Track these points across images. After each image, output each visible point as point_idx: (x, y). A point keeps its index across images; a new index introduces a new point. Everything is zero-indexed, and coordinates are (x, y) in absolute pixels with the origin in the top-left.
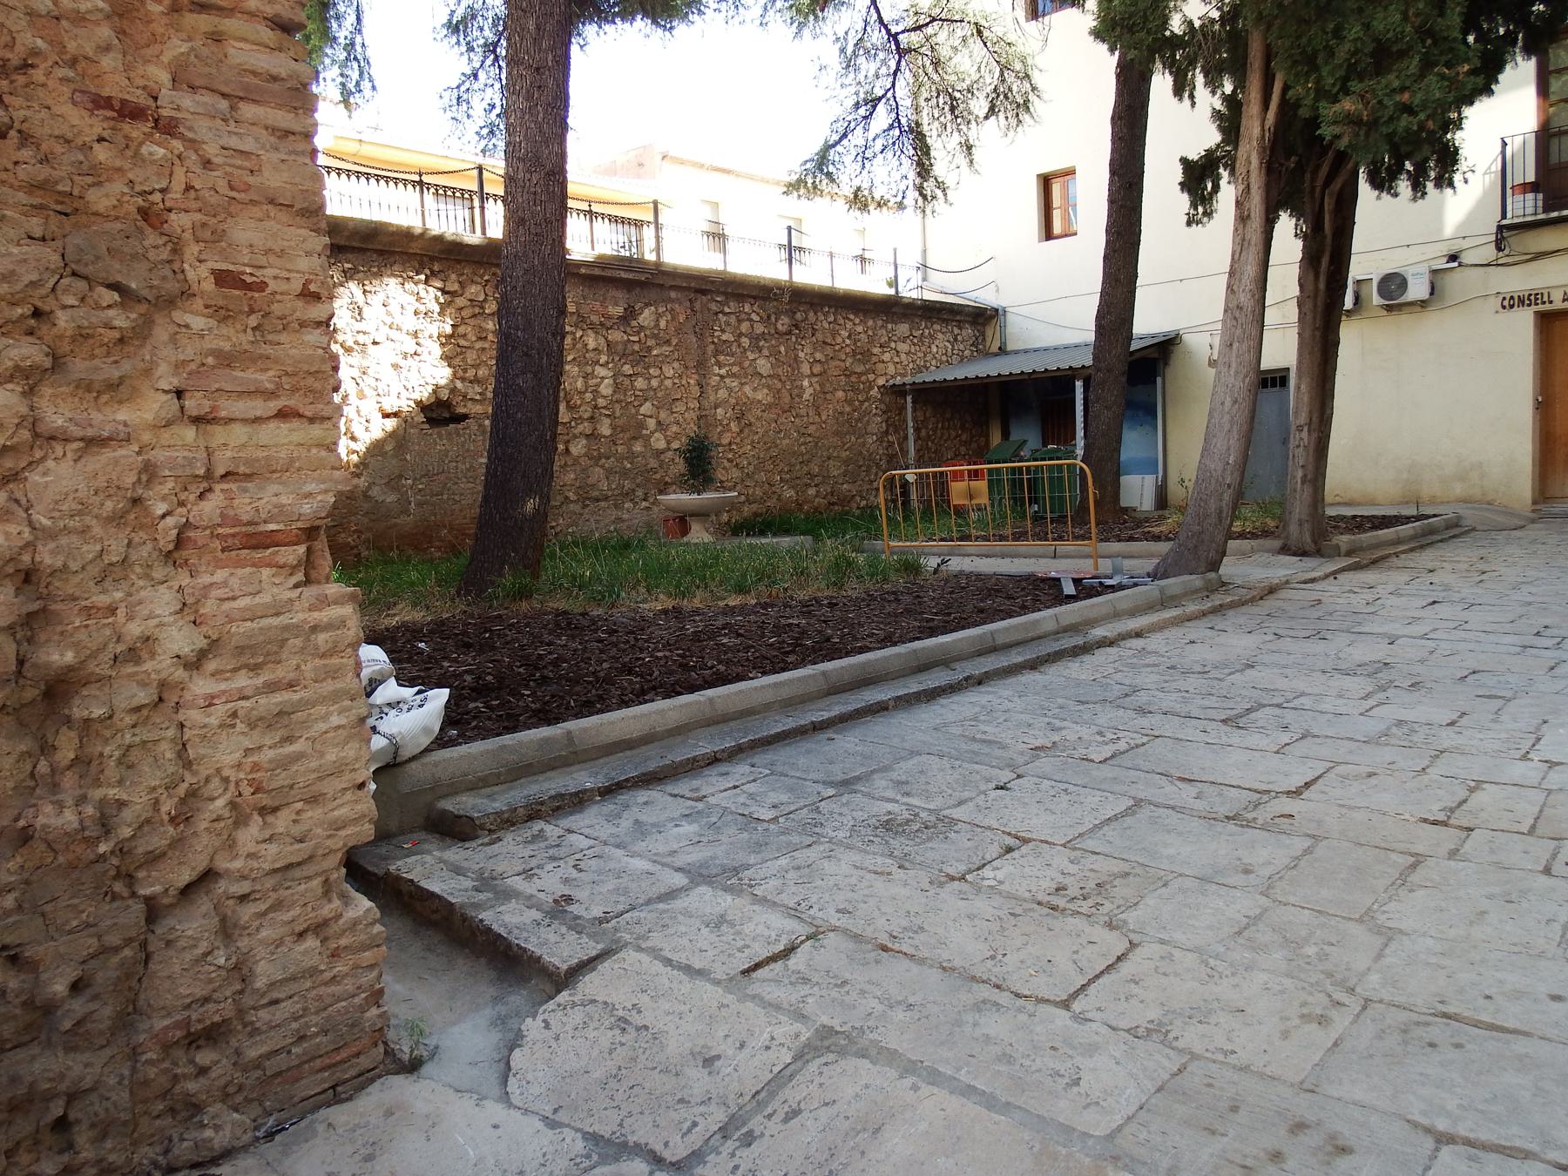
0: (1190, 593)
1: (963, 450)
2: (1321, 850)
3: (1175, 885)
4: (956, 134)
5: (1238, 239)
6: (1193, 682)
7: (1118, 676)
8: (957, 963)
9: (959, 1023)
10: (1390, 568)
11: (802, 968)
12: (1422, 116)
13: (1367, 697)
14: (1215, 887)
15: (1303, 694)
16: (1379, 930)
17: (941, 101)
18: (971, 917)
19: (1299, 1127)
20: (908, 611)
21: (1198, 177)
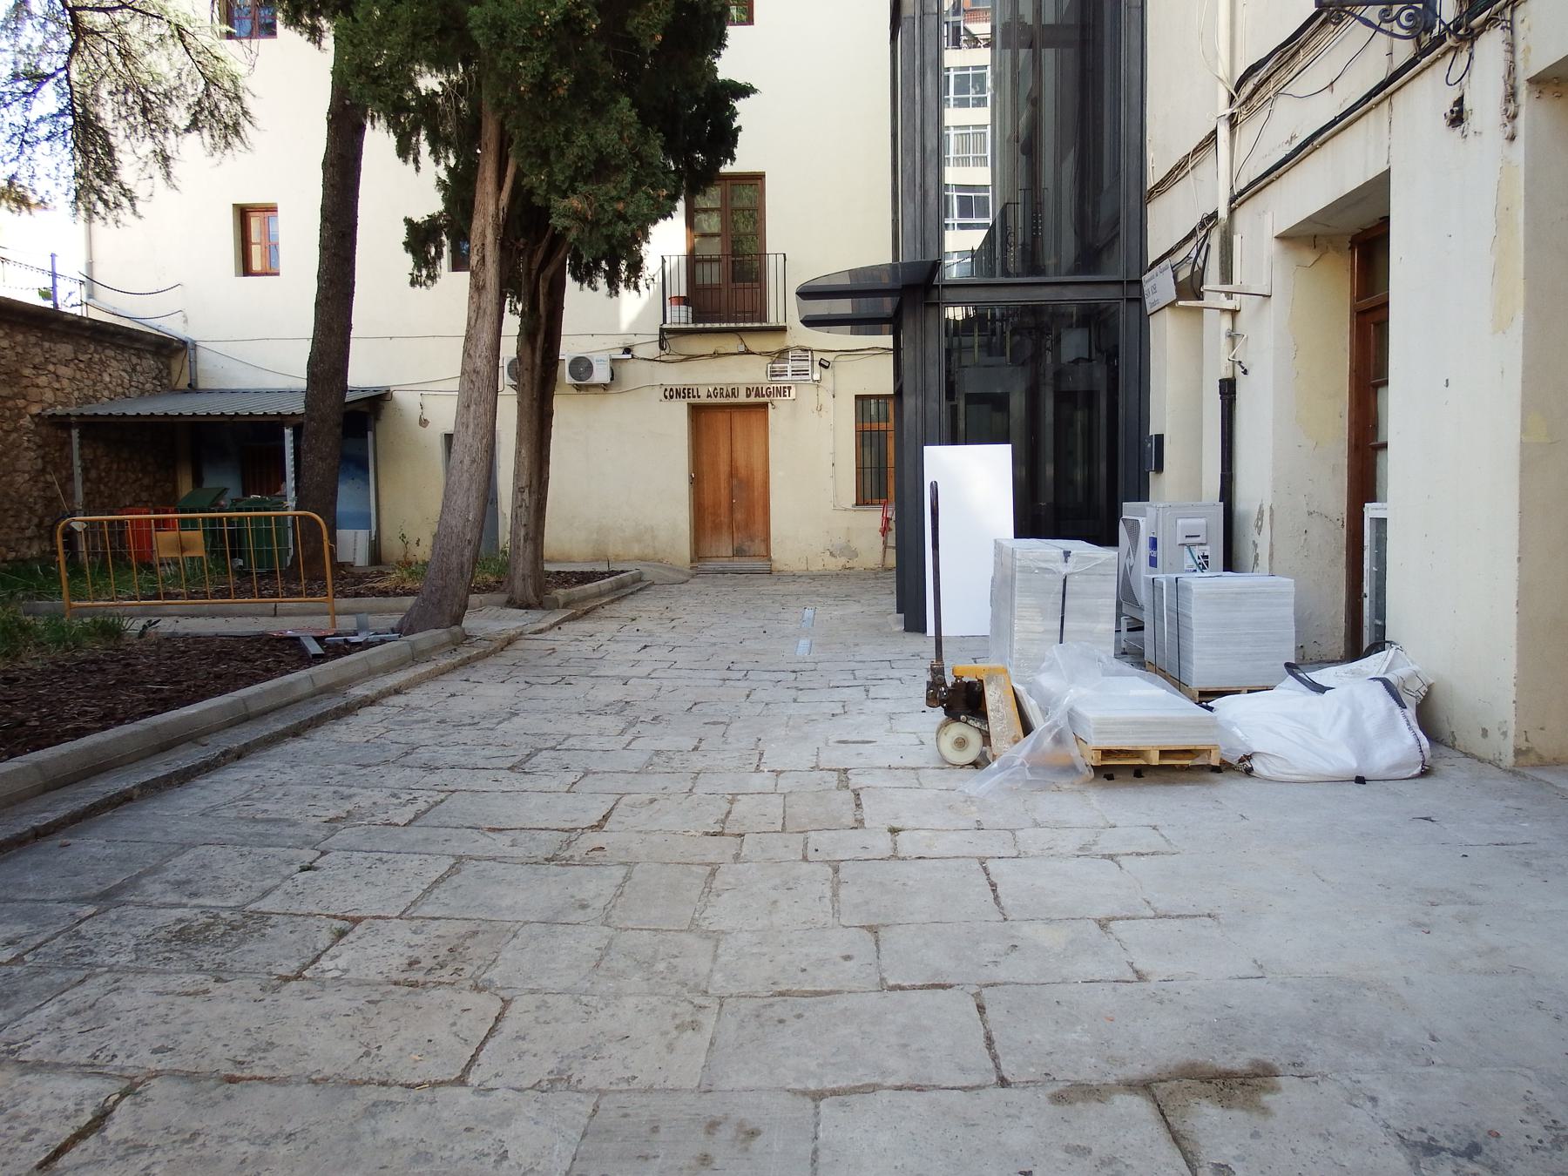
0: (438, 647)
1: (144, 496)
2: (637, 875)
3: (524, 933)
4: (148, 139)
5: (473, 307)
6: (467, 734)
7: (391, 735)
8: (328, 1071)
9: (355, 1137)
11: (129, 1134)
12: (634, 225)
13: (622, 733)
14: (560, 928)
15: (569, 736)
16: (707, 935)
17: (130, 99)
18: (326, 1016)
19: (712, 1126)
20: (122, 683)
21: (420, 239)
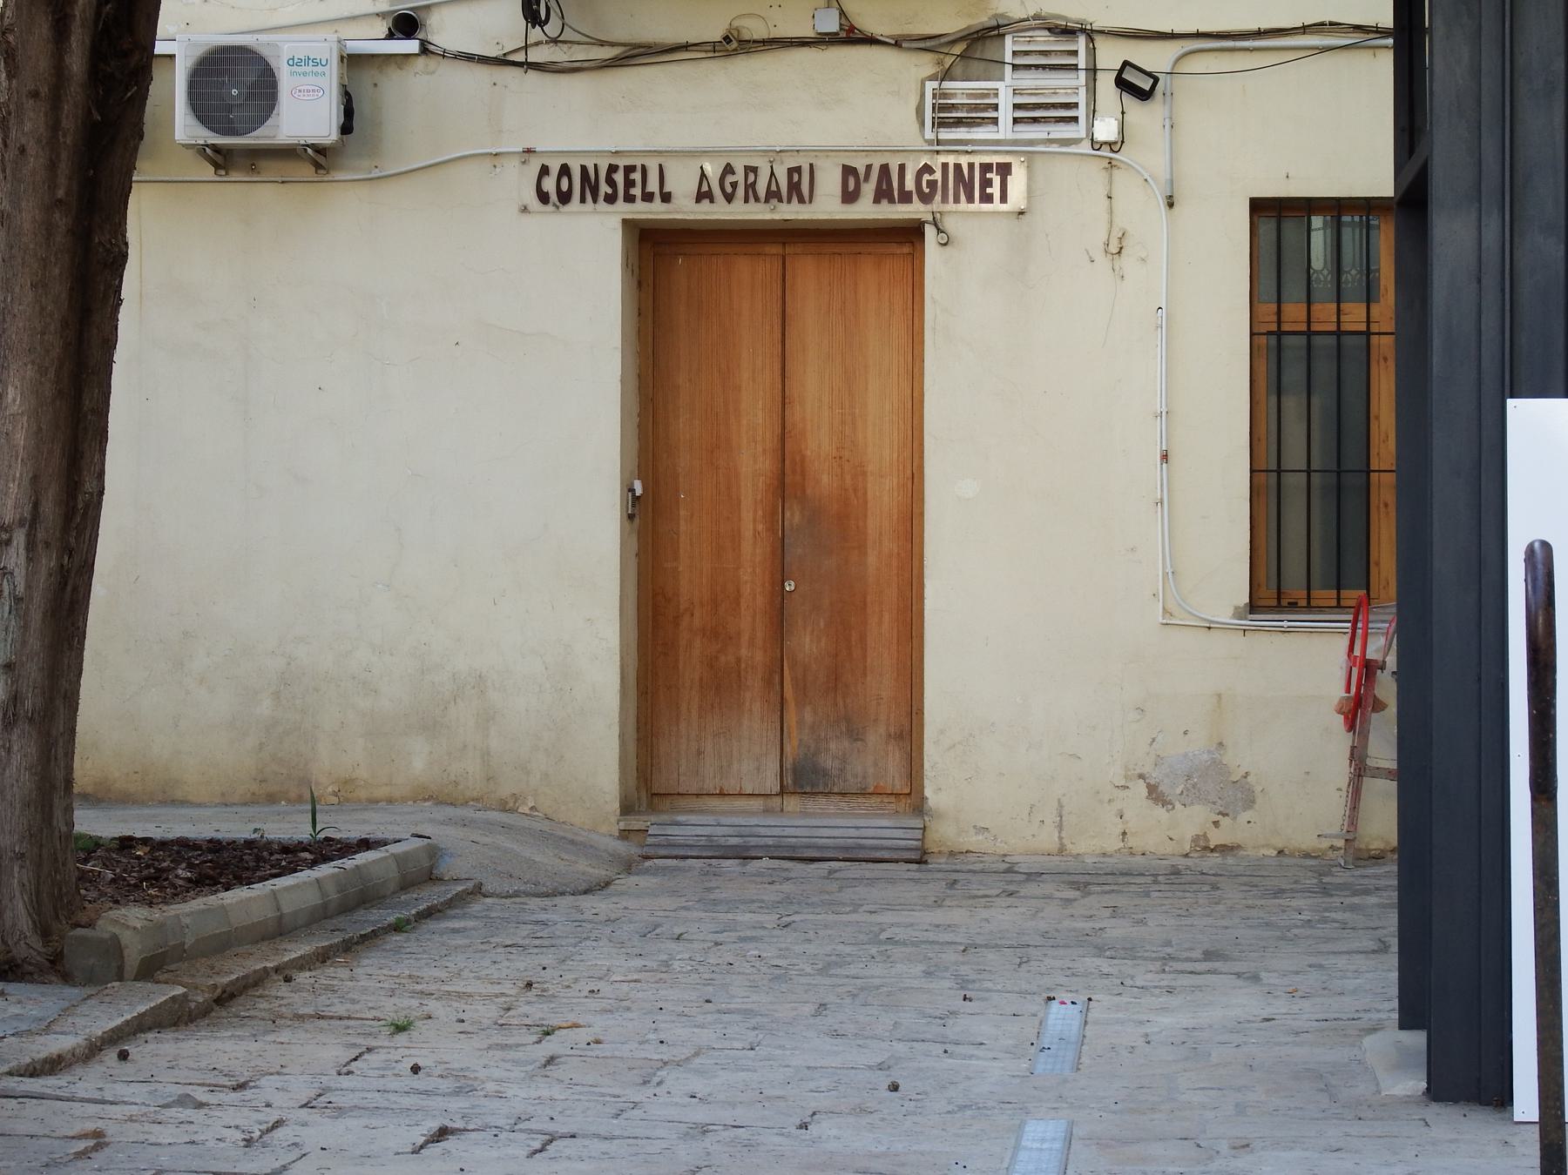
10: (275, 1019)
